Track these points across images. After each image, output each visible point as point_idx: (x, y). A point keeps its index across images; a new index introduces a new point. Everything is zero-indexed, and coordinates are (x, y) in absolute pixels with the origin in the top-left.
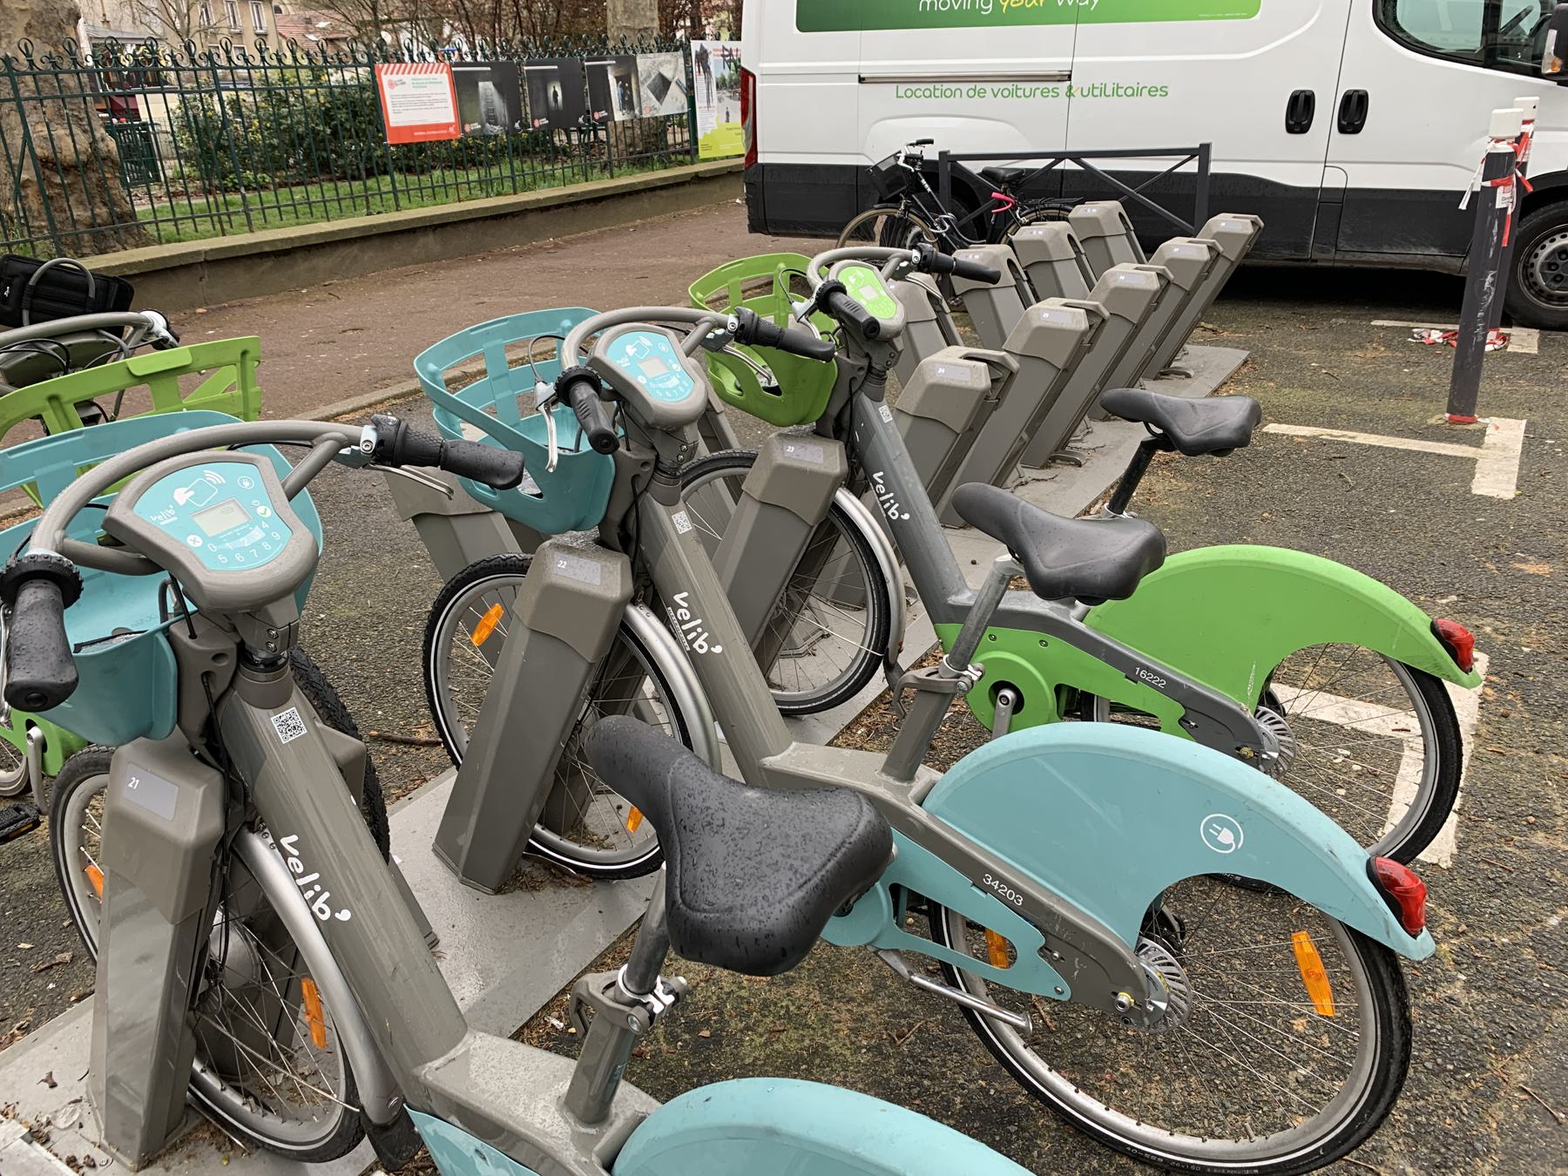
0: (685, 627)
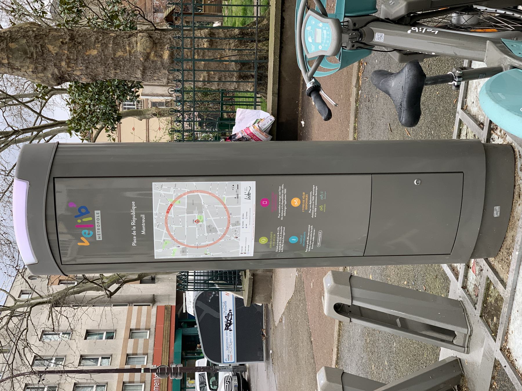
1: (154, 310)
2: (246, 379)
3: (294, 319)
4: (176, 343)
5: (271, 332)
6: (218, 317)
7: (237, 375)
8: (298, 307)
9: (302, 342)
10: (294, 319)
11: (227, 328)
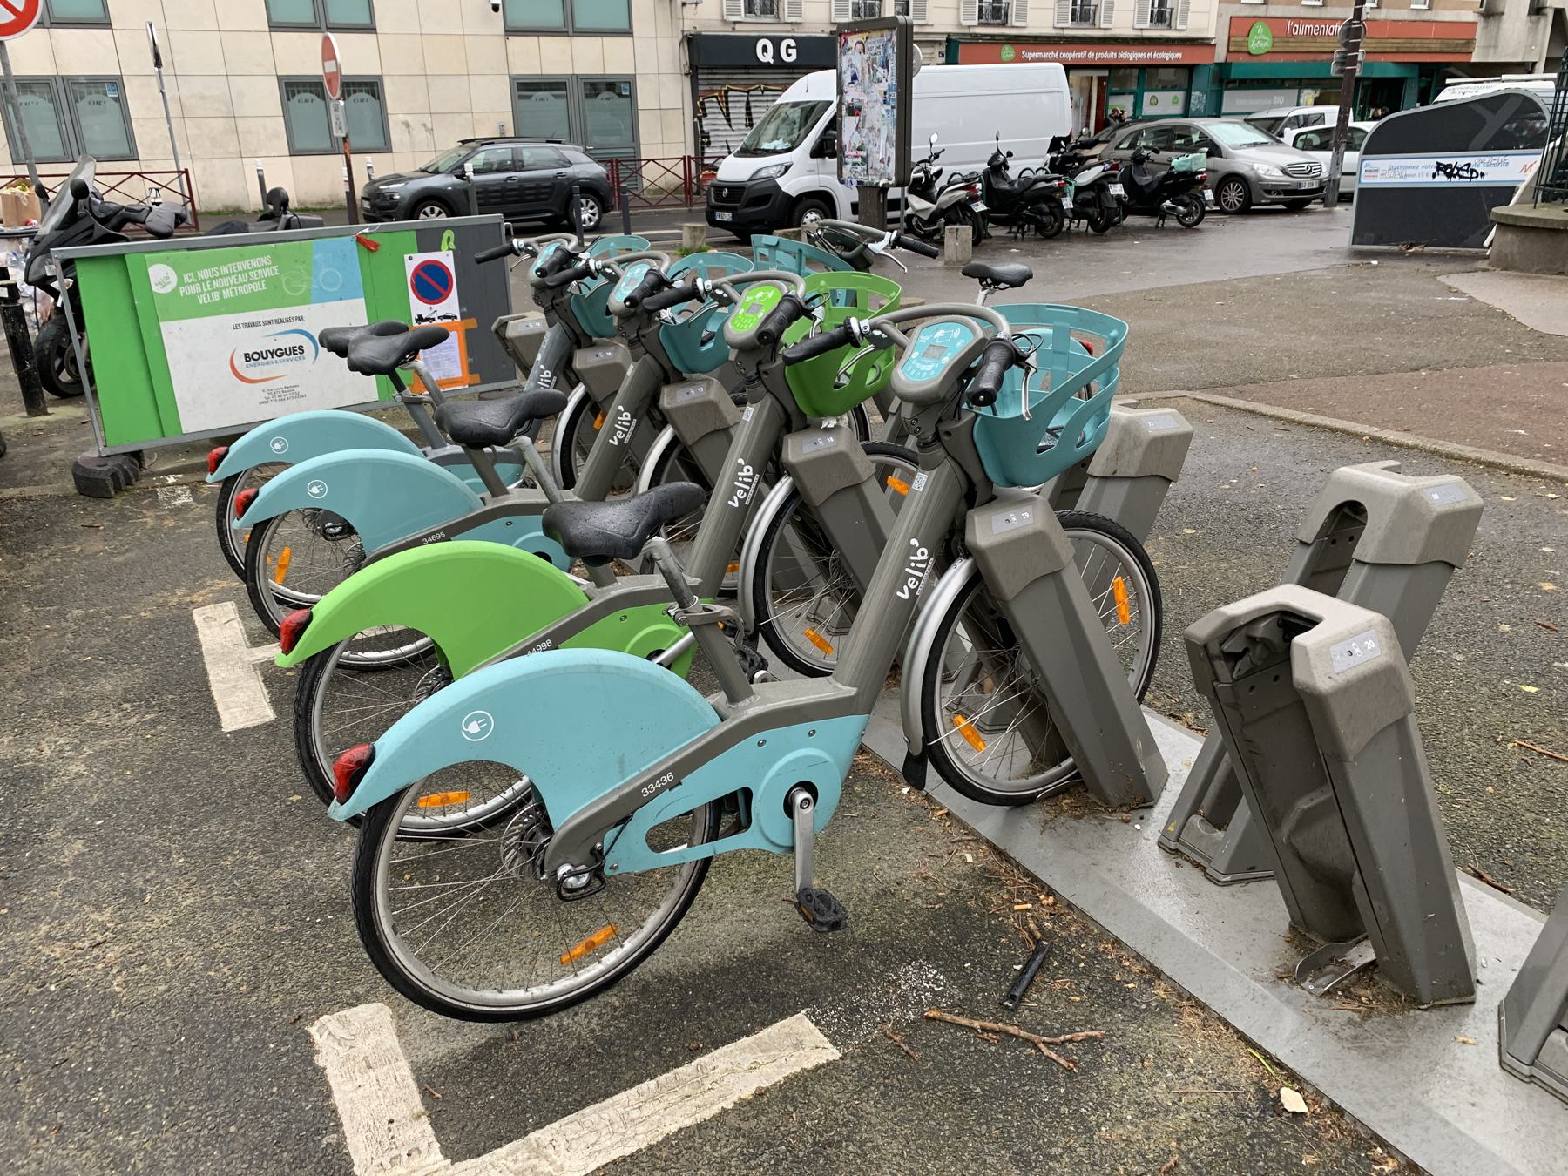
0: (920, 574)
1: (1469, 16)
2: (1310, 206)
3: (1465, 325)
4: (1392, 66)
5: (1420, 265)
6: (1470, 147)
7: (1321, 189)
8: (1501, 340)
9: (1412, 344)
10: (1465, 325)
11: (1439, 167)
